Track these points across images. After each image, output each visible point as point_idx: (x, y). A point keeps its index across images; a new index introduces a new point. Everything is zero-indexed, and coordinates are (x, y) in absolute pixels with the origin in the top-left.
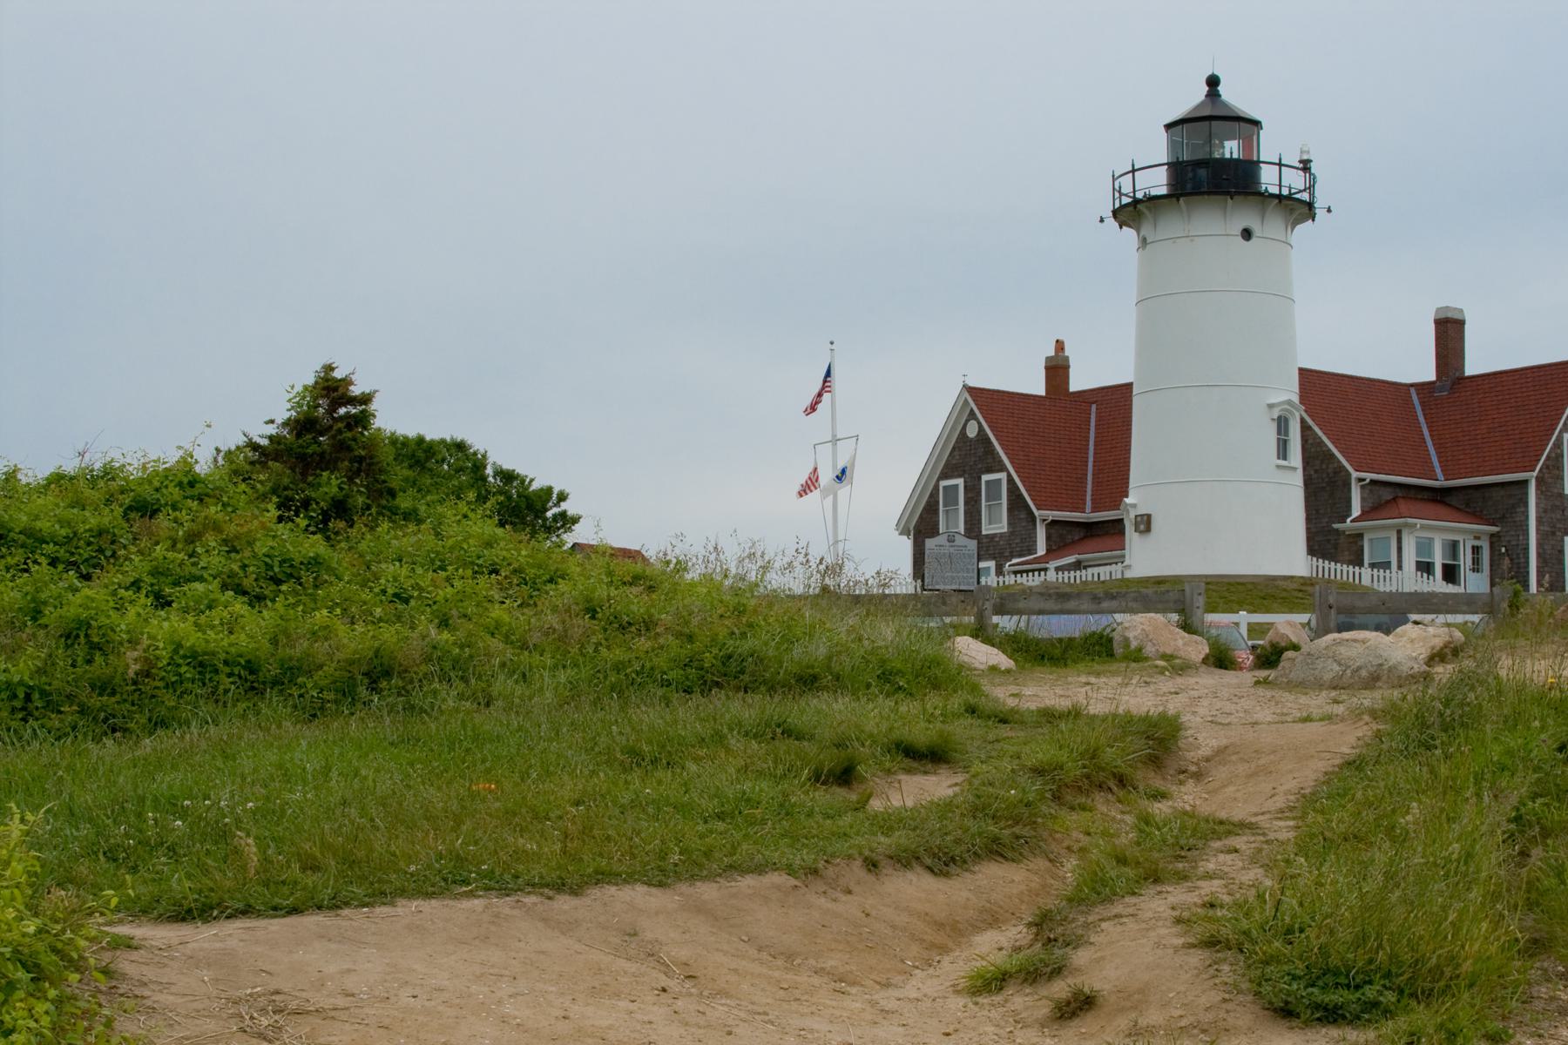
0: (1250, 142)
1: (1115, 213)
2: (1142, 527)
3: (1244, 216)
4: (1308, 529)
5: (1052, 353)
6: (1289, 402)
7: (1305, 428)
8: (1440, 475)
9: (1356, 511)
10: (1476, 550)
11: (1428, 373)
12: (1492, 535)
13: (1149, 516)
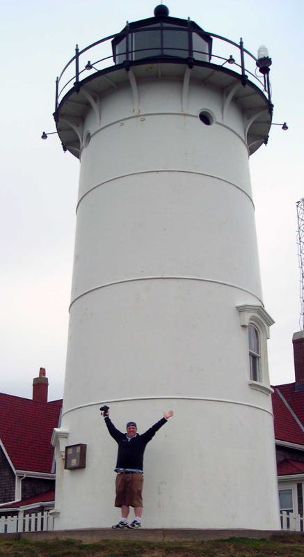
2: (74, 462)
5: (37, 376)
13: (83, 448)
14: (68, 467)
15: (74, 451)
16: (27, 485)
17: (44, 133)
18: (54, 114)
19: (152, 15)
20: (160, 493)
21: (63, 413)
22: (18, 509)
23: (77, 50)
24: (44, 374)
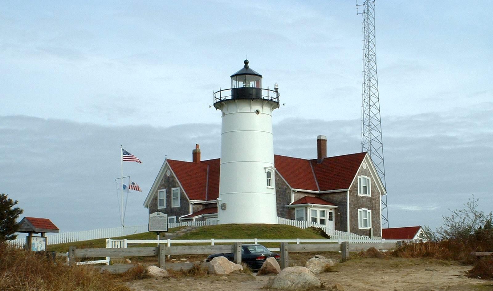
0: (258, 83)
1: (214, 104)
4: (277, 207)
5: (195, 149)
6: (271, 167)
7: (276, 174)
8: (319, 190)
10: (331, 214)
11: (315, 157)
12: (335, 209)
16: (195, 207)
19: (244, 64)
22: (193, 218)
23: (220, 89)
24: (198, 147)
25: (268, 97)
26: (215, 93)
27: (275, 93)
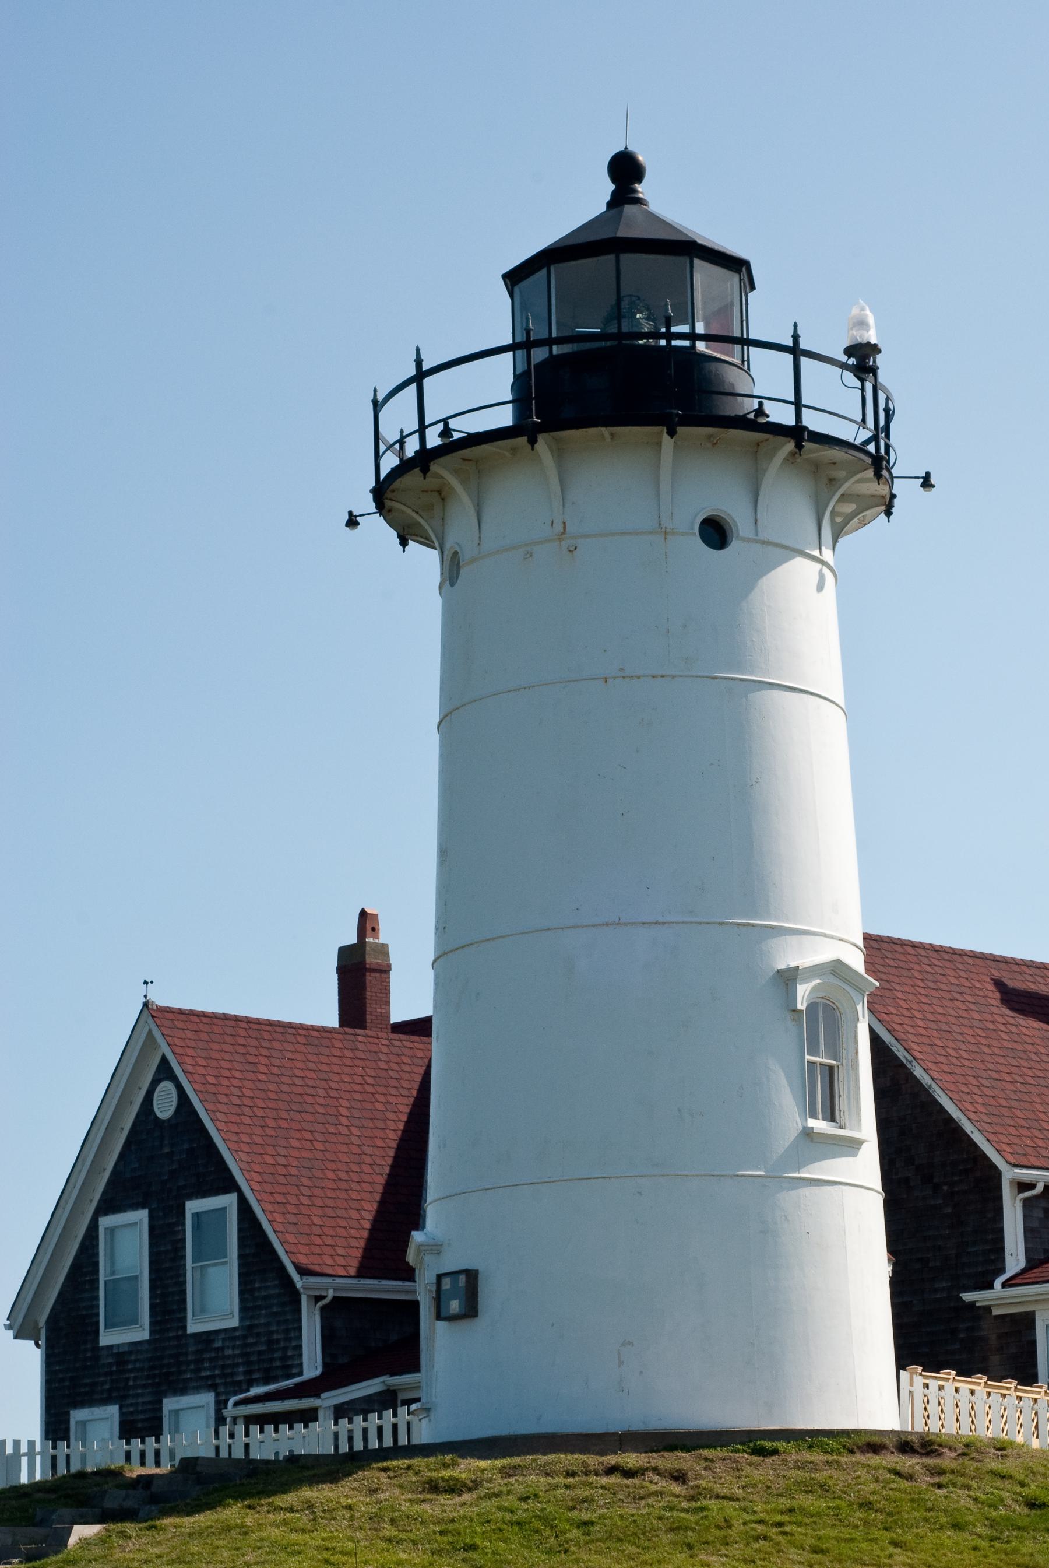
2: (455, 1306)
3: (699, 479)
5: (352, 939)
9: (1015, 1258)
13: (472, 1276)
14: (443, 1315)
15: (454, 1284)
17: (350, 513)
18: (372, 491)
20: (621, 1363)
21: (429, 1200)
23: (419, 362)
25: (798, 404)
26: (380, 398)
27: (850, 378)
